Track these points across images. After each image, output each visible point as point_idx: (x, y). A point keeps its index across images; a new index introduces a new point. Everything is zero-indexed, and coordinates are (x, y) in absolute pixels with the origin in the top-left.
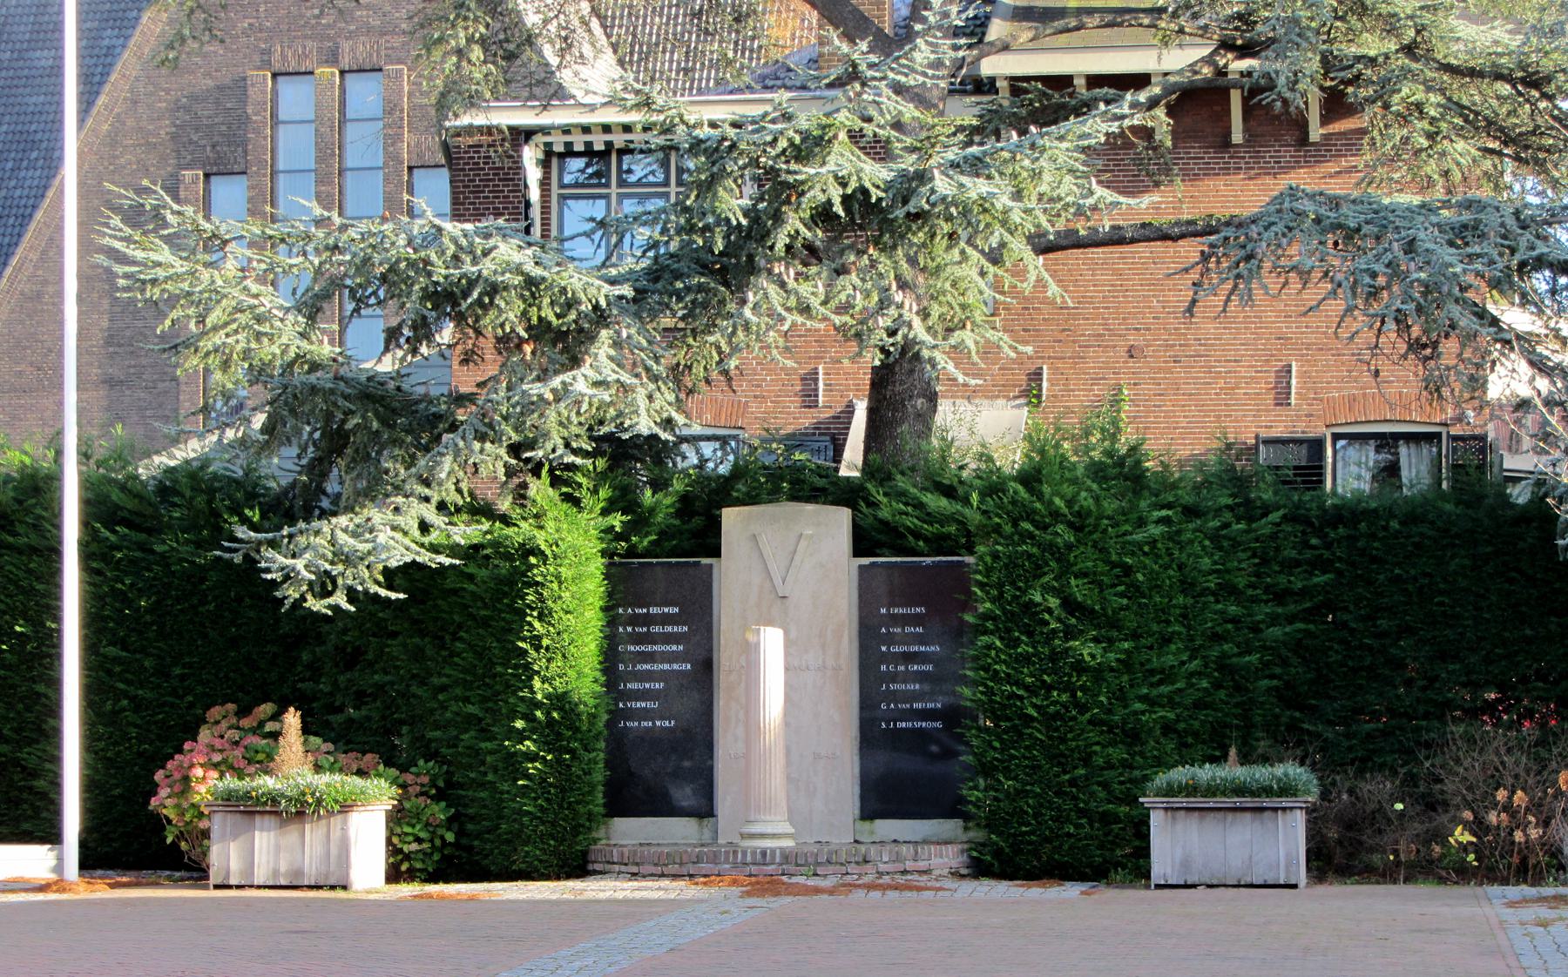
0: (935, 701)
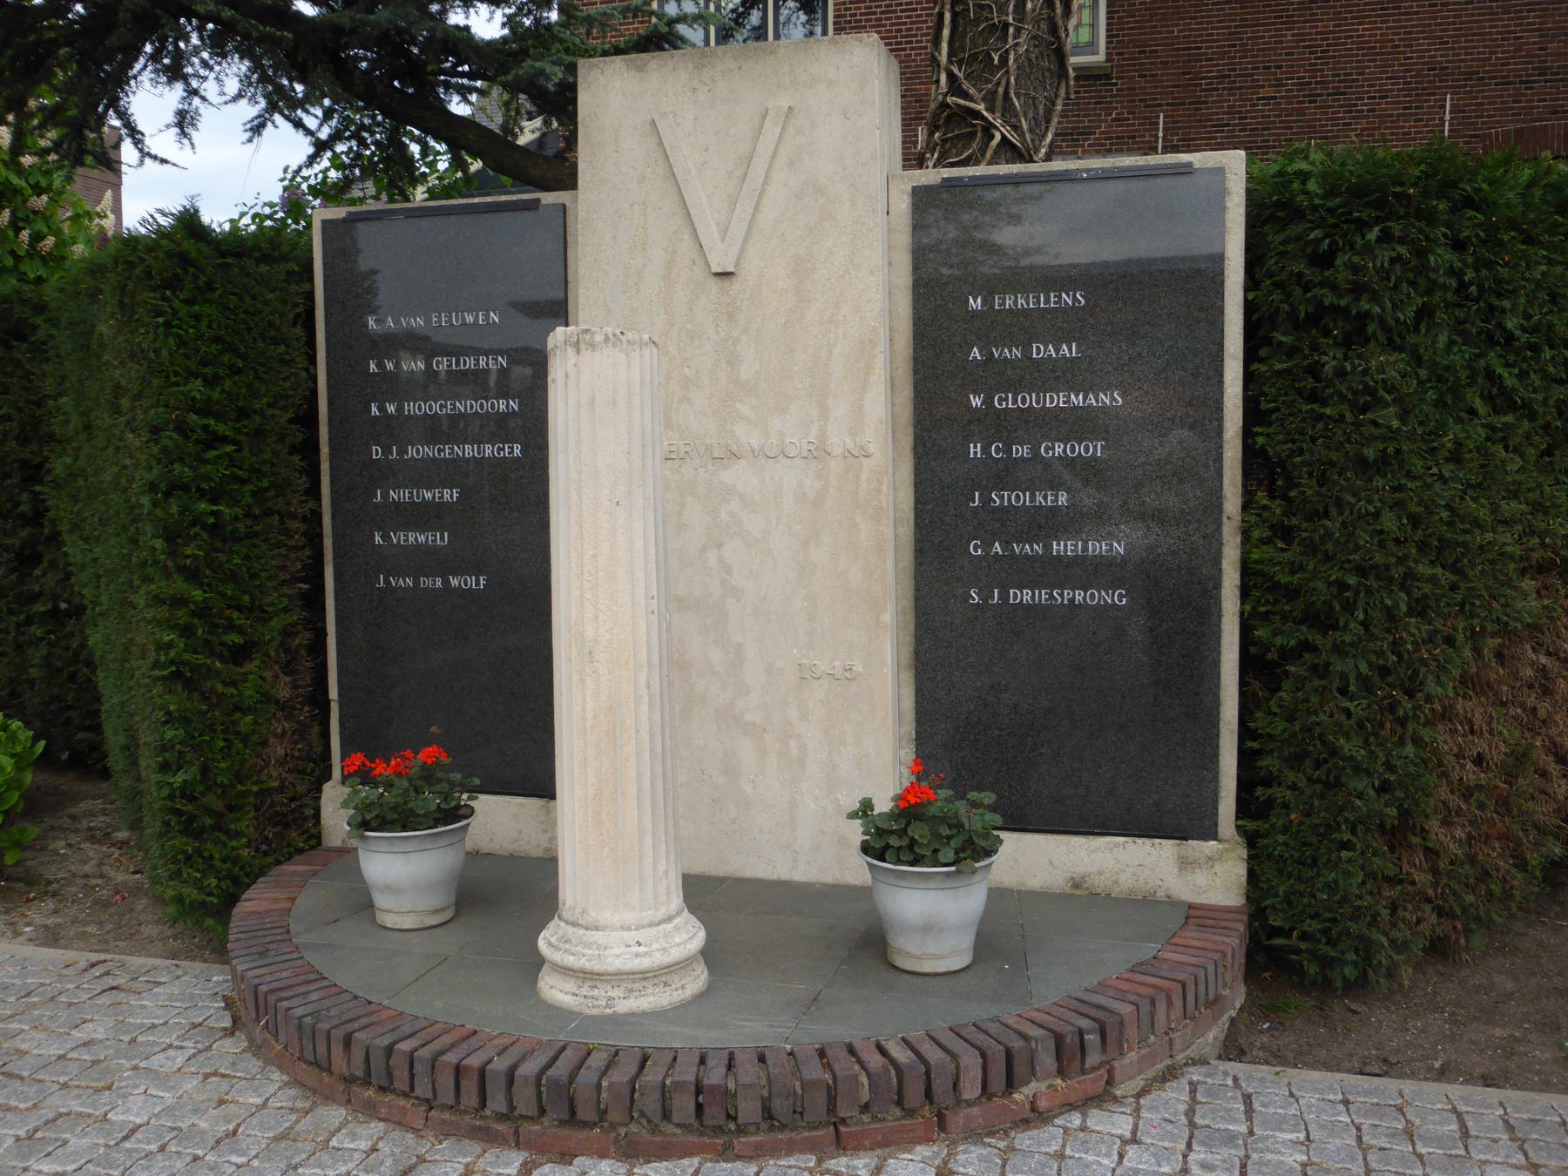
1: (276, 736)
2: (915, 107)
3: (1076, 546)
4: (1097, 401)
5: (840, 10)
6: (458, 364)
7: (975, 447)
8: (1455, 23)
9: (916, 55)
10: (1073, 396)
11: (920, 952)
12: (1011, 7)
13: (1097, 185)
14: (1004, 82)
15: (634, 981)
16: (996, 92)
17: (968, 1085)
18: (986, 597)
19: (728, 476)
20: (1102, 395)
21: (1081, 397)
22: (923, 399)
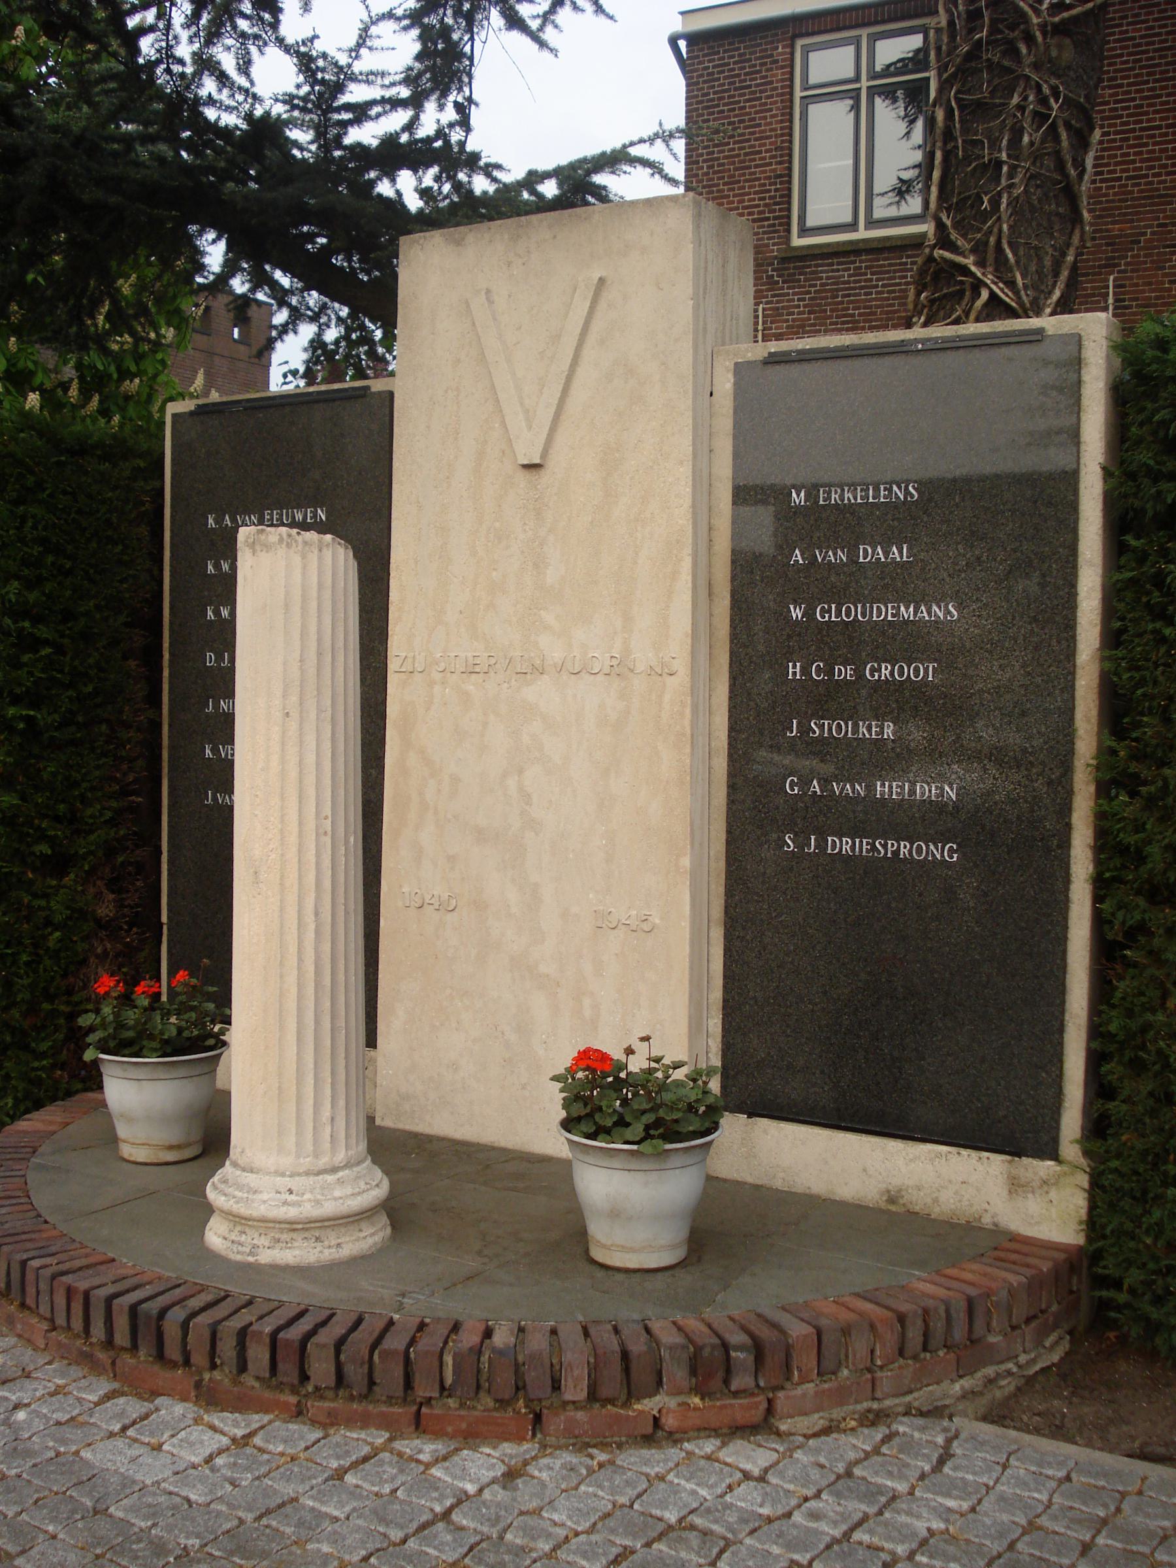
0: (941, 778)
1: (97, 956)
2: (1106, 252)
3: (902, 788)
4: (929, 613)
5: (692, 170)
7: (794, 667)
9: (1108, 188)
10: (902, 608)
11: (609, 1243)
12: (1005, 142)
13: (934, 357)
14: (995, 230)
15: (281, 1231)
16: (987, 243)
17: (570, 1383)
18: (802, 844)
19: (530, 693)
20: (935, 608)
21: (911, 609)
22: (740, 609)
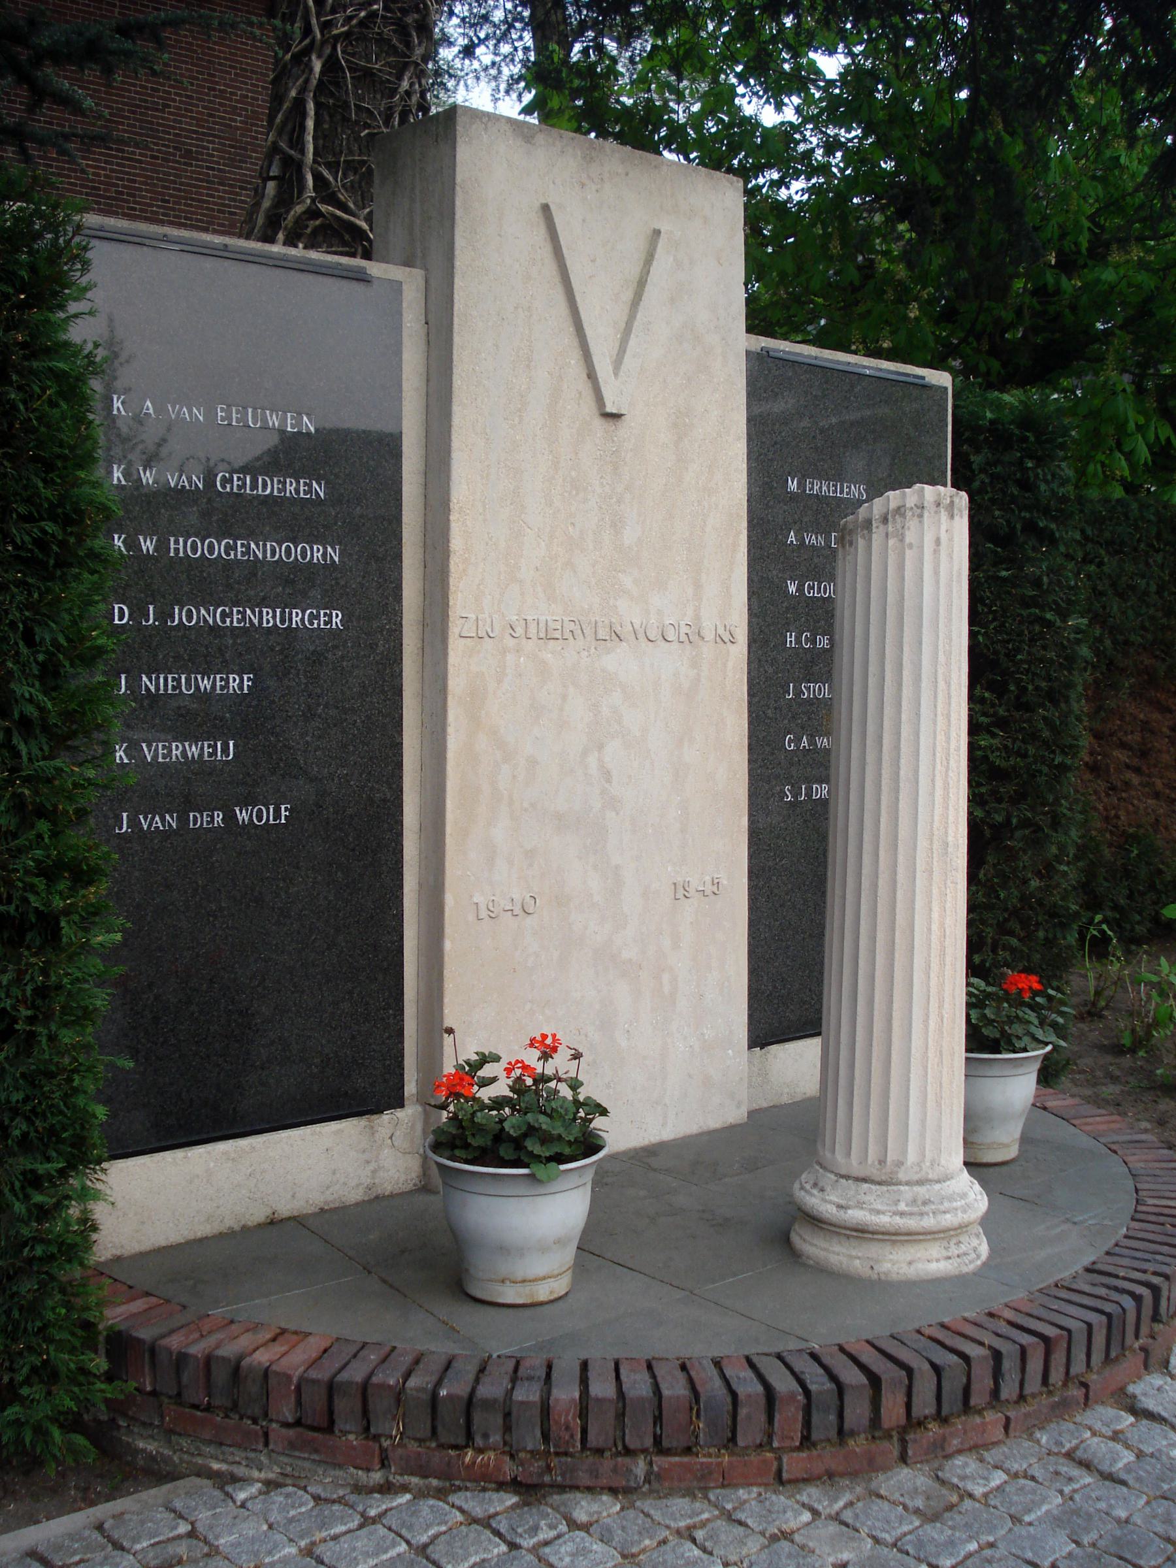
6: (254, 486)
8: (175, 183)
